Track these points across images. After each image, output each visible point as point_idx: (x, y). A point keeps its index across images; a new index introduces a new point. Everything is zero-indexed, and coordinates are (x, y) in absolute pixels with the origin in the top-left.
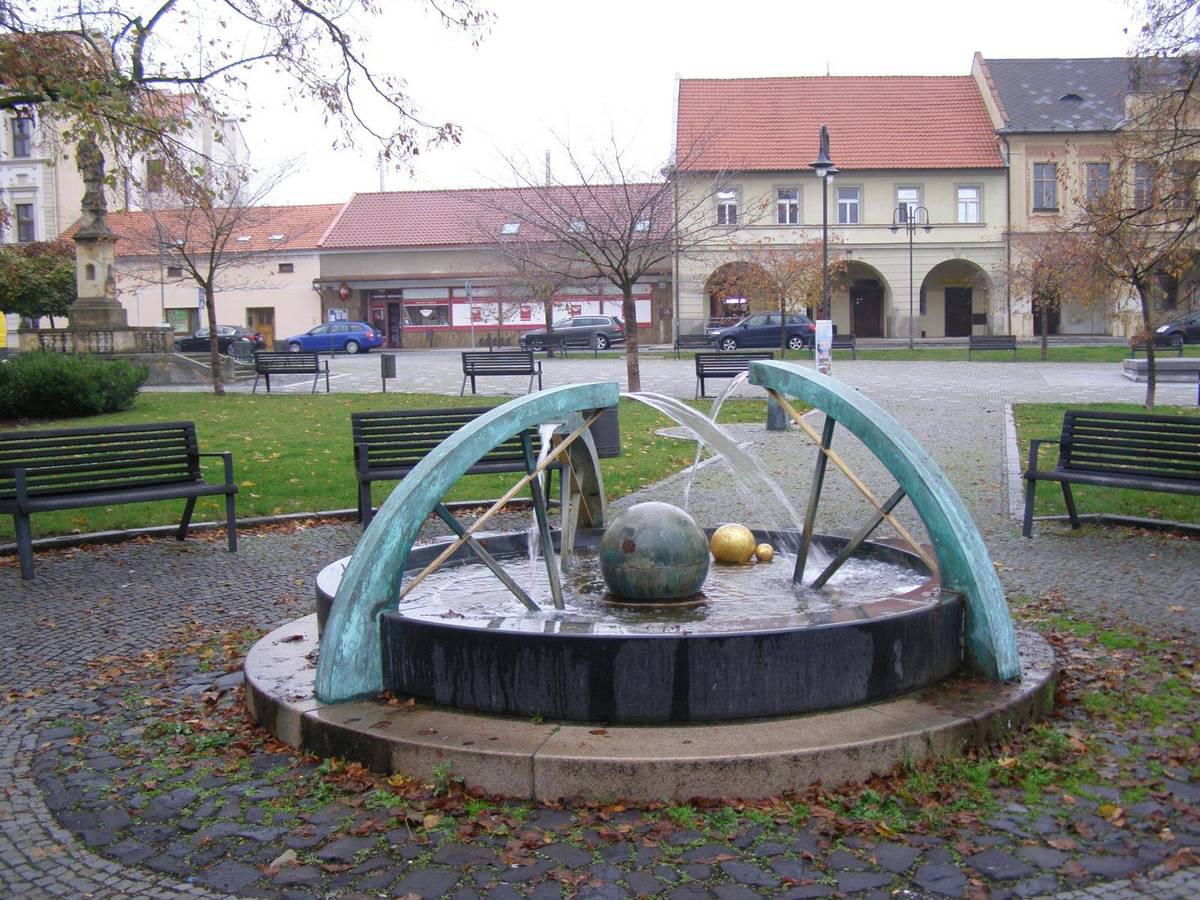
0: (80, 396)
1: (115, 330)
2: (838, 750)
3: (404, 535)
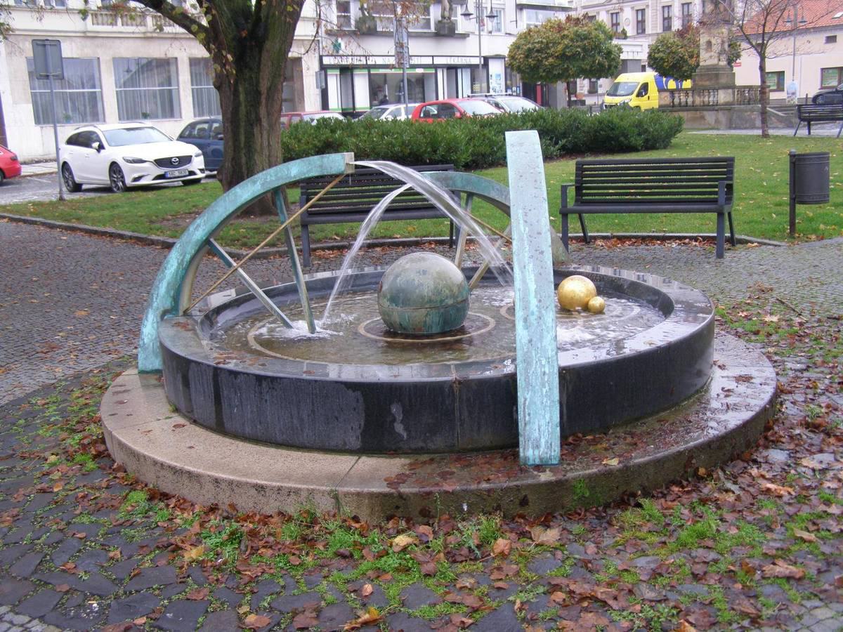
0: (622, 139)
1: (720, 88)
2: (247, 483)
3: (179, 264)
